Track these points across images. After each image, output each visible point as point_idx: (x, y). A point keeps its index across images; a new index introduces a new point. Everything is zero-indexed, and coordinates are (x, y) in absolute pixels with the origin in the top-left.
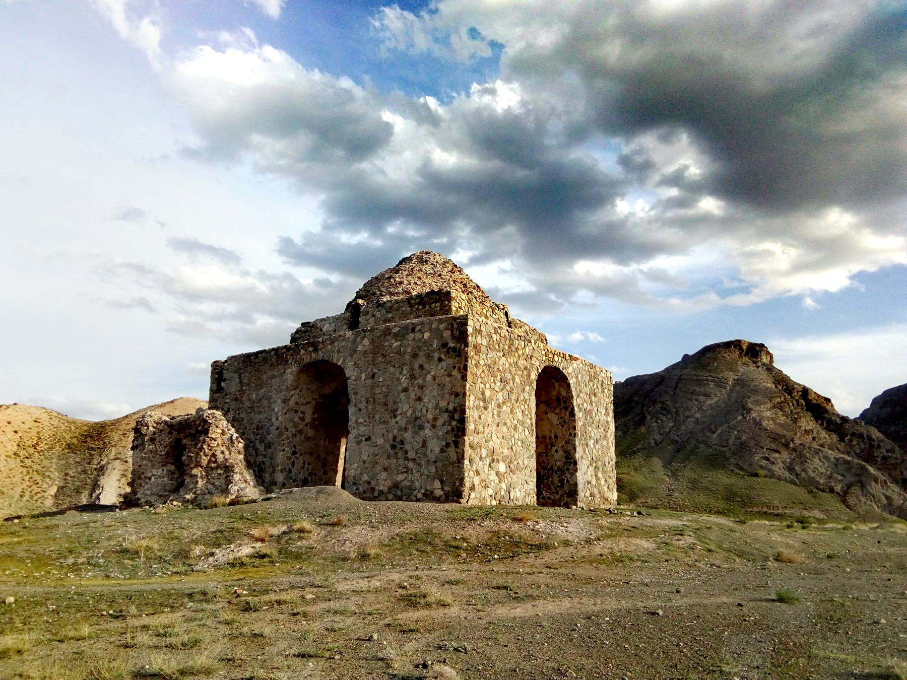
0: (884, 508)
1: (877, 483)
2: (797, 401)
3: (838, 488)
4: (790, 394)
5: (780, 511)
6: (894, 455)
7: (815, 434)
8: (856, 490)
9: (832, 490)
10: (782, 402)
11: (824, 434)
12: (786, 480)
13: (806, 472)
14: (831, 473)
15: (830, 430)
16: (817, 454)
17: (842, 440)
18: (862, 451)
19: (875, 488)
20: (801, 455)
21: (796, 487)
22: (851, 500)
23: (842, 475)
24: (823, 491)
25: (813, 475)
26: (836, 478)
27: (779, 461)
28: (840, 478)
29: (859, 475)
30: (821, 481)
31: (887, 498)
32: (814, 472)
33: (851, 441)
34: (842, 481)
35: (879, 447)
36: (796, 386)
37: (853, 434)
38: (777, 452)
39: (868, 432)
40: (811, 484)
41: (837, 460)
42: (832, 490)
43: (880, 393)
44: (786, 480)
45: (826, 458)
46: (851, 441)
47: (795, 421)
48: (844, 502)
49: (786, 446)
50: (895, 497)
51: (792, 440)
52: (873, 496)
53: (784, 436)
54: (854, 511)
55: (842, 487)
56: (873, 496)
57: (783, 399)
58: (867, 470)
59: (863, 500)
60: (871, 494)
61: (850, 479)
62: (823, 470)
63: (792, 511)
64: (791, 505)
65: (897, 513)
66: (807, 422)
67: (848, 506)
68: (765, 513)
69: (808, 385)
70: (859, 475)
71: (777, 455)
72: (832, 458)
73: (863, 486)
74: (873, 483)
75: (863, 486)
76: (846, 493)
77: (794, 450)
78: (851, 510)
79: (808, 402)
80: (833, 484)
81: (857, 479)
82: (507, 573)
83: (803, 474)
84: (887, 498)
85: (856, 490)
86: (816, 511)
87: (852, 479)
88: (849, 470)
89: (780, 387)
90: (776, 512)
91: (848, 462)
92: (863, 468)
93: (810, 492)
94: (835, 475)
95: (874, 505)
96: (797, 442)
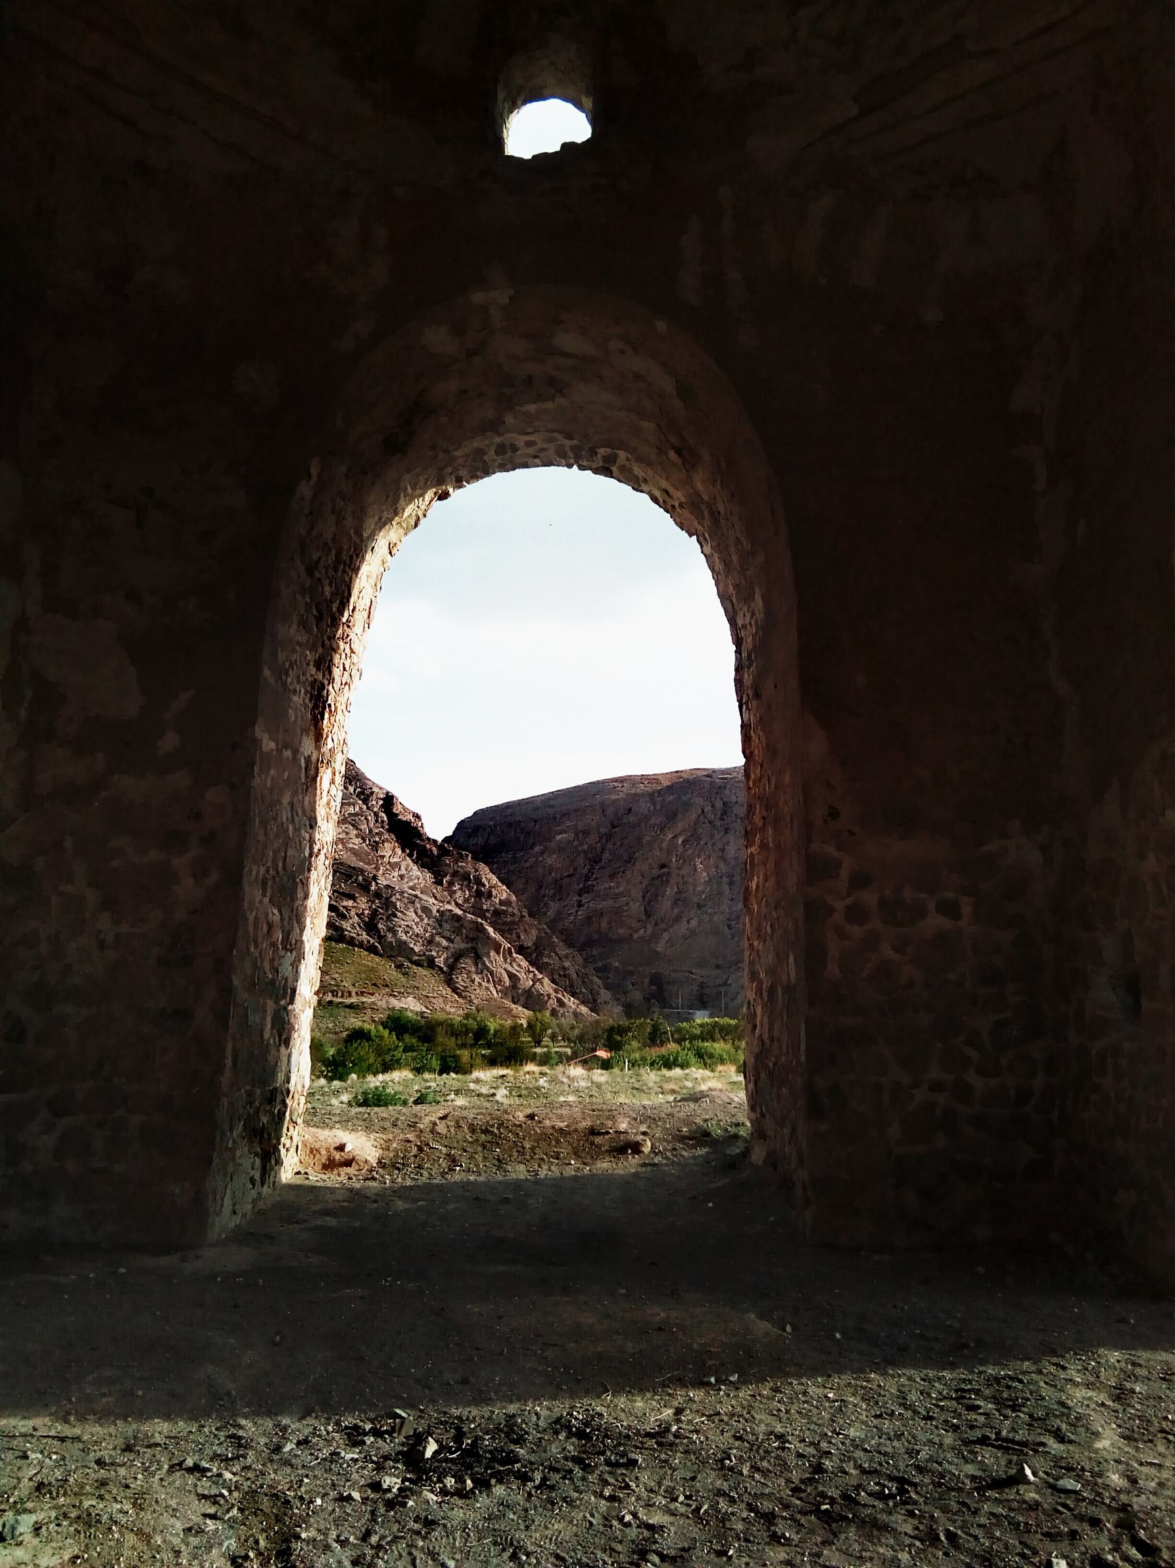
0: (504, 993)
1: (498, 953)
2: (376, 814)
3: (440, 962)
4: (365, 801)
5: (353, 1000)
6: (510, 910)
7: (403, 872)
8: (467, 963)
9: (431, 964)
10: (356, 814)
11: (415, 871)
12: (361, 945)
13: (395, 933)
14: (432, 936)
15: (423, 866)
16: (413, 903)
17: (439, 882)
18: (466, 900)
19: (496, 962)
20: (388, 904)
21: (377, 959)
22: (460, 980)
23: (448, 939)
24: (418, 964)
25: (404, 938)
26: (439, 944)
27: (353, 913)
28: (445, 943)
29: (473, 939)
30: (416, 949)
31: (511, 976)
32: (406, 933)
33: (451, 884)
34: (447, 948)
35: (490, 895)
36: (375, 790)
37: (455, 874)
38: (351, 897)
39: (476, 870)
40: (399, 954)
41: (441, 913)
42: (431, 964)
43: (470, 814)
44: (361, 945)
45: (426, 910)
46: (451, 884)
47: (375, 847)
48: (450, 983)
49: (365, 888)
50: (522, 976)
51: (375, 878)
52: (492, 974)
53: (362, 871)
54: (464, 998)
55: (446, 959)
56: (492, 973)
57: (357, 809)
58: (484, 931)
59: (477, 979)
60: (488, 969)
61: (460, 944)
62: (418, 930)
63: (373, 999)
64: (371, 989)
65: (522, 999)
66: (391, 851)
67: (455, 990)
68: (330, 1002)
69: (394, 791)
70: (473, 939)
71: (350, 903)
72: (434, 912)
73: (478, 958)
74: (492, 953)
75: (478, 958)
76: (452, 967)
77: (378, 895)
78: (460, 996)
79: (392, 816)
80: (434, 953)
81: (470, 945)
82: (62, 1439)
83: (390, 935)
84: (511, 976)
85: (467, 963)
86: (410, 999)
87: (463, 946)
88: (457, 931)
89: (351, 789)
90: (348, 1001)
91: (457, 918)
92: (480, 929)
93: (399, 967)
94: (437, 938)
95: (492, 989)
96: (383, 881)
